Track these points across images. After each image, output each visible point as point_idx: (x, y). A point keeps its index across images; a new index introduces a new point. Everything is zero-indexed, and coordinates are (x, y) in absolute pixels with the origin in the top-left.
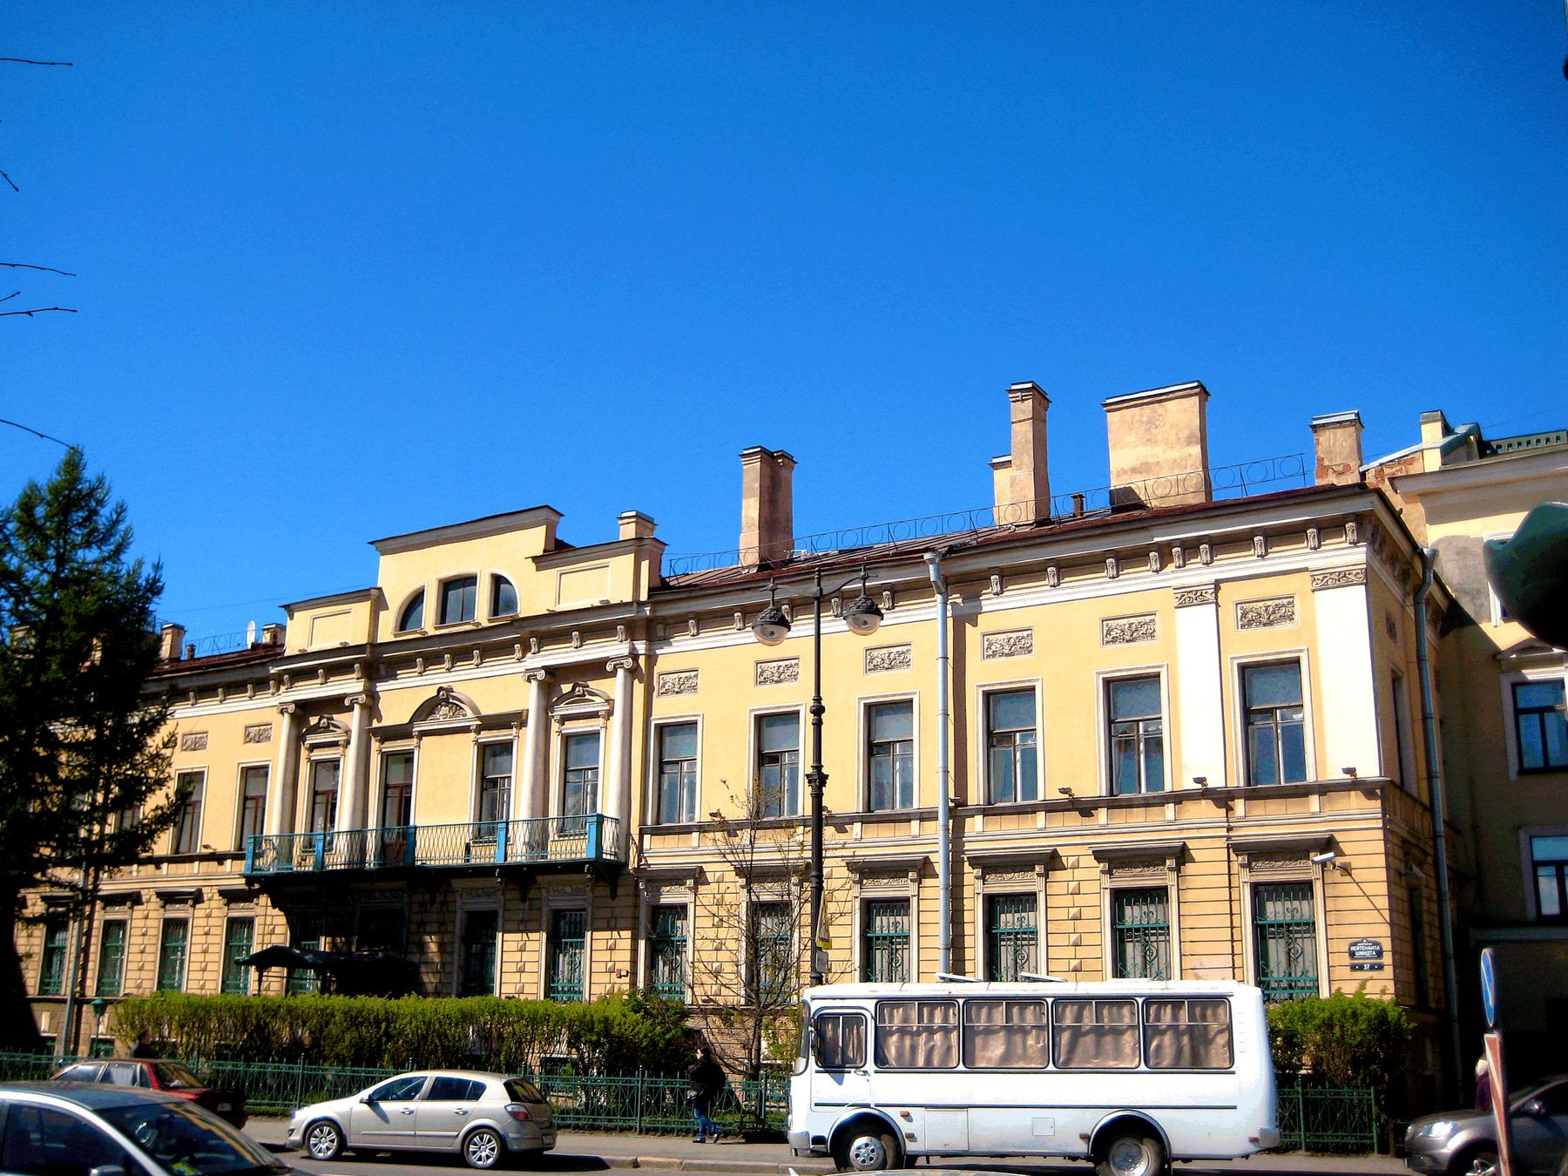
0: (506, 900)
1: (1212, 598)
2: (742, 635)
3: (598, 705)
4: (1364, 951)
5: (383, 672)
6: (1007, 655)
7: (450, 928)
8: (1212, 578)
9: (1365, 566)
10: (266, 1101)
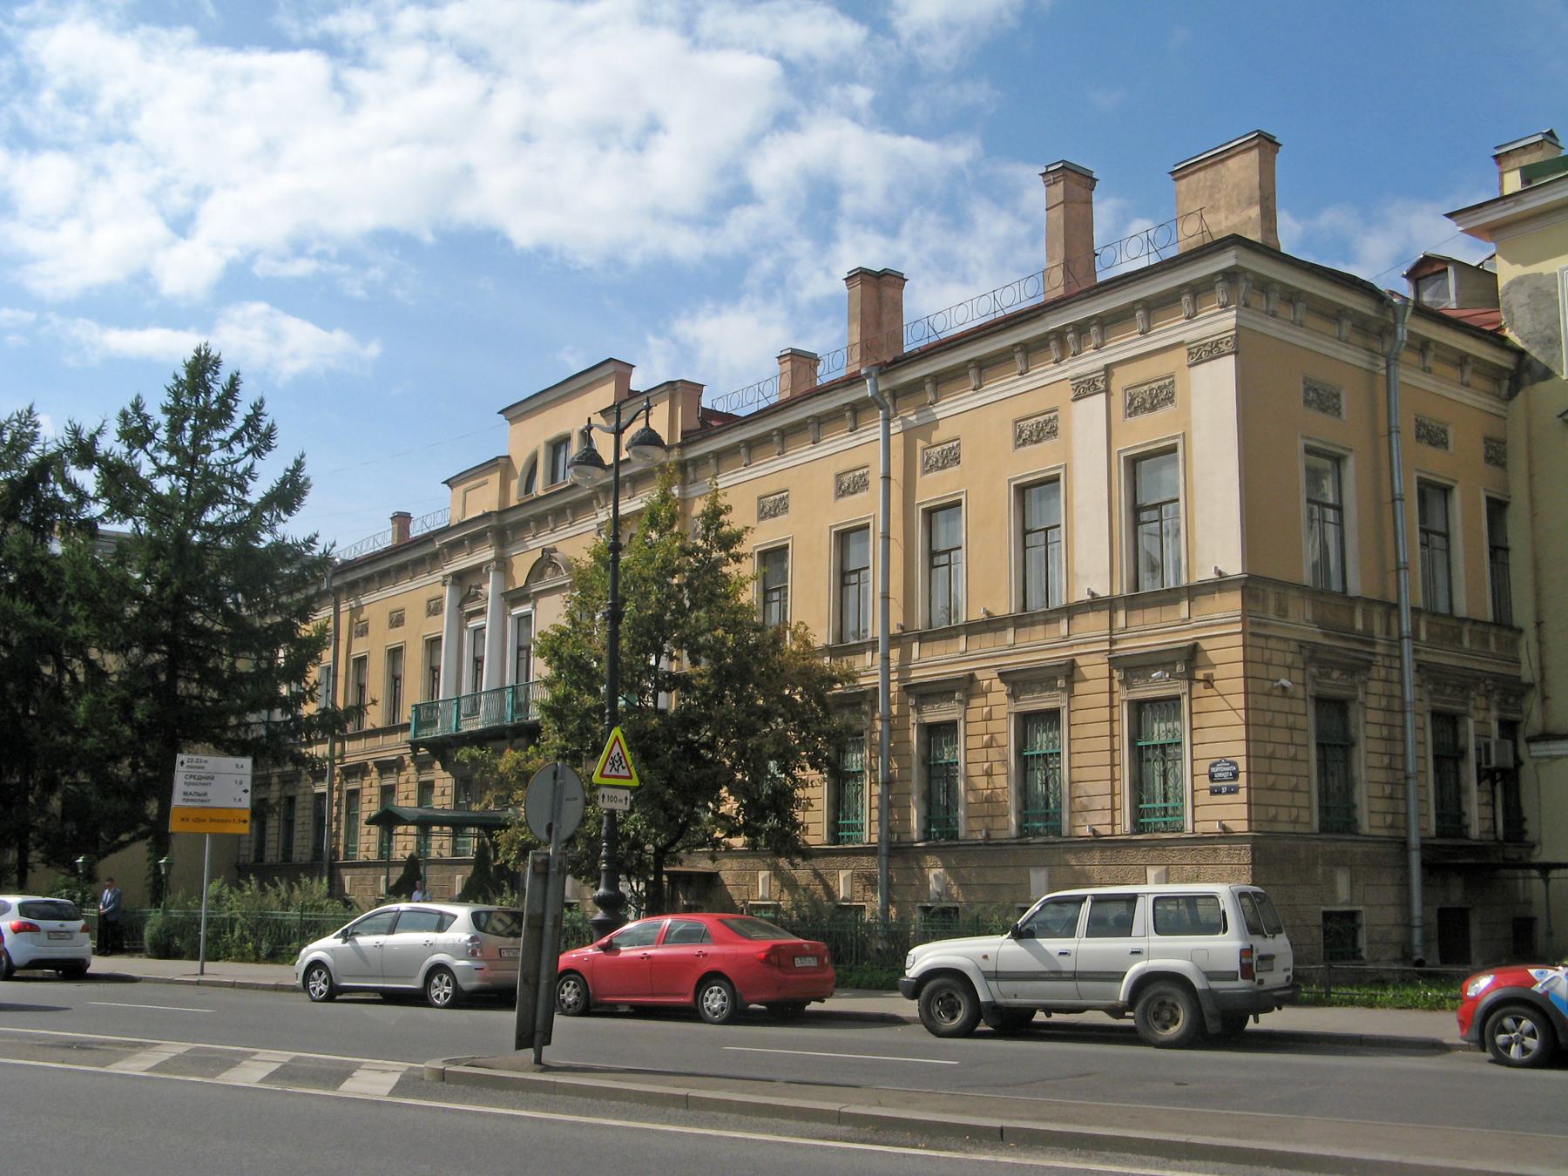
1: (1101, 386)
2: (749, 471)
4: (1222, 771)
8: (1101, 364)
9: (1234, 332)
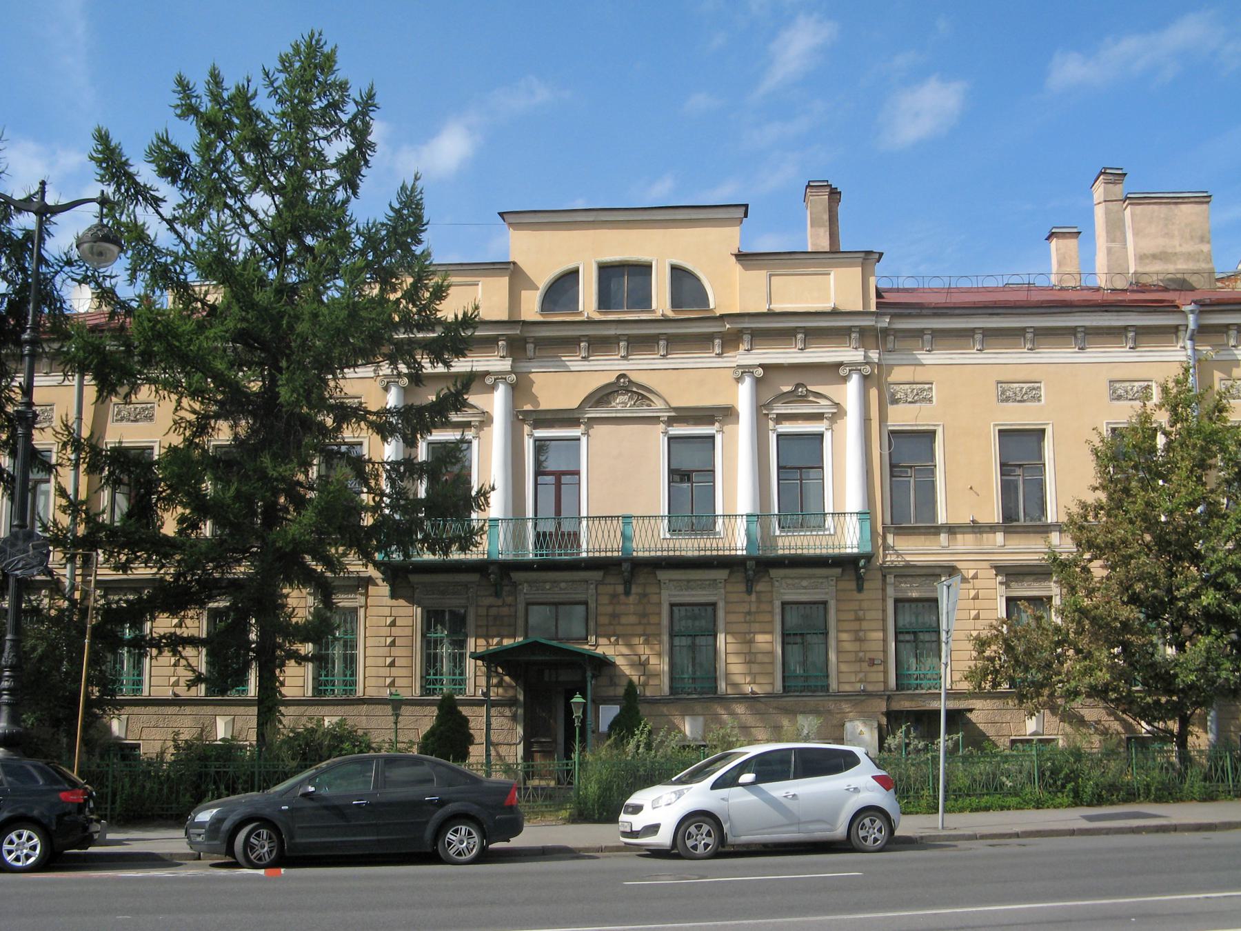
0: (727, 592)
3: (823, 406)
5: (530, 353)
6: (910, 402)
7: (654, 619)
10: (109, 806)
